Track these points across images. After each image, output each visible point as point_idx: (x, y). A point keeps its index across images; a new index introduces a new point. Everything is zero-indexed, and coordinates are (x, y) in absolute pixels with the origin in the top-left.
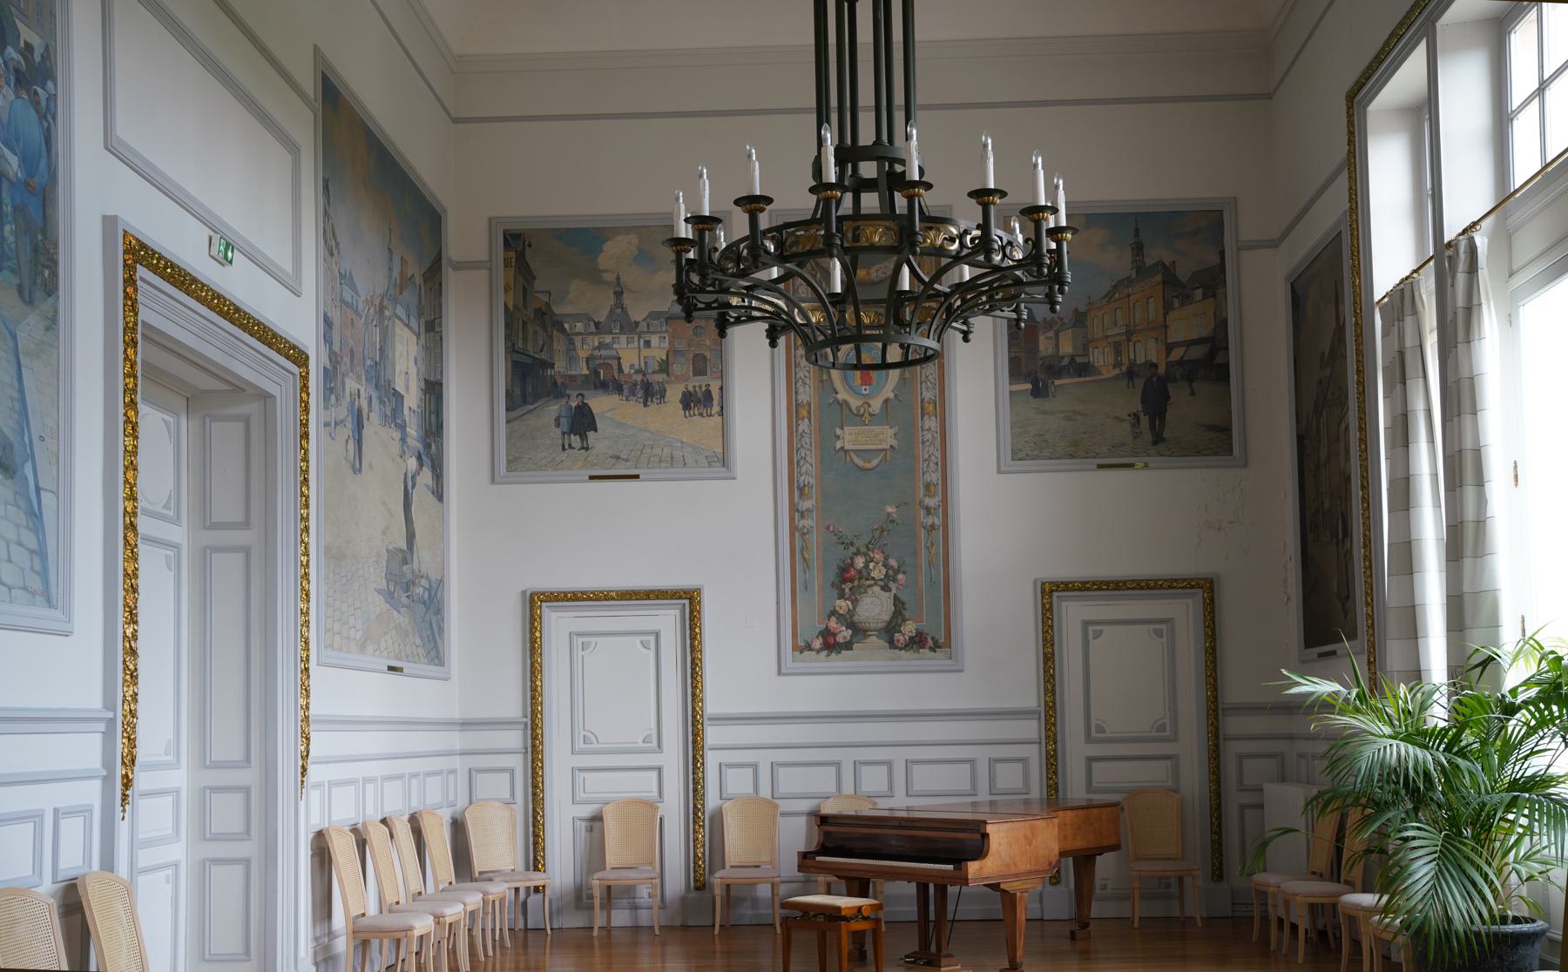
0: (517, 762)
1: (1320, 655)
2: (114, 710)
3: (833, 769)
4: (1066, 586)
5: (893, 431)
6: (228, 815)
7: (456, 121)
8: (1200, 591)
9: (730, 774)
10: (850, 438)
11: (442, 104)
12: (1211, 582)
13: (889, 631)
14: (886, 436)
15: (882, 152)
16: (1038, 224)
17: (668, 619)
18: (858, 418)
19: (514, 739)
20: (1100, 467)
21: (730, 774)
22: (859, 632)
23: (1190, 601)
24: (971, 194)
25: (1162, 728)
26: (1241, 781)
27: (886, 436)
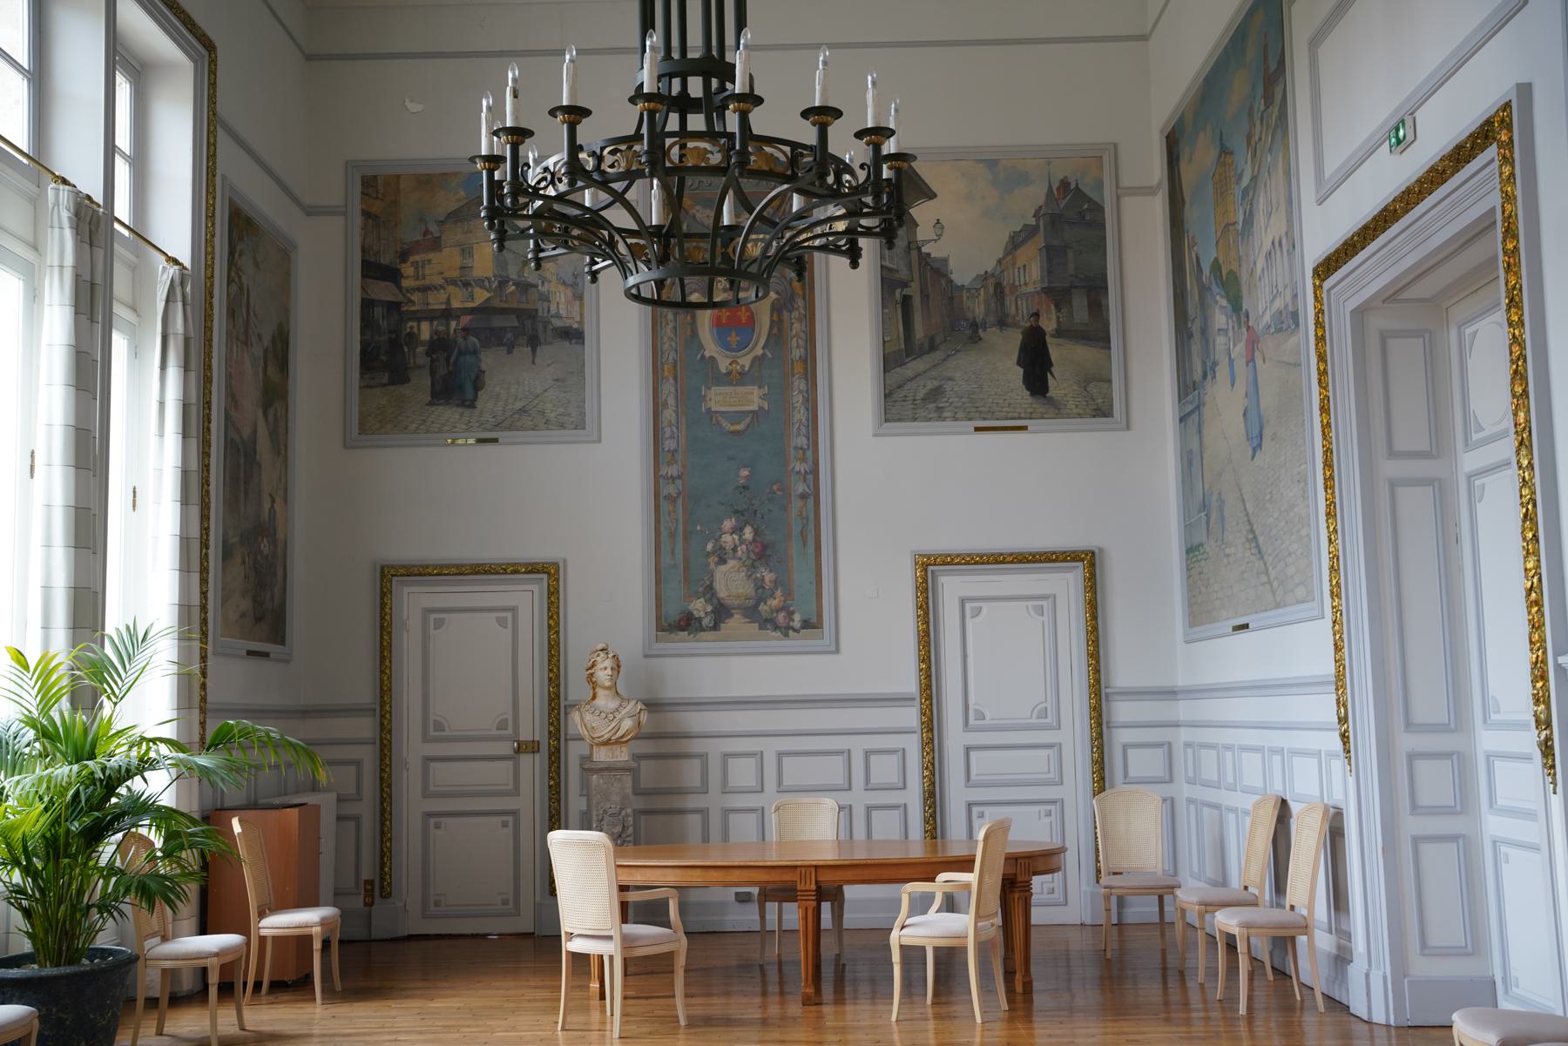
0: (912, 744)
1: (250, 653)
2: (1558, 666)
3: (873, 758)
4: (950, 561)
5: (762, 392)
6: (1435, 783)
7: (309, 58)
8: (545, 576)
9: (894, 760)
10: (719, 399)
11: (289, 33)
12: (556, 565)
13: (751, 613)
14: (752, 398)
15: (716, 67)
16: (877, 148)
17: (952, 587)
18: (730, 379)
19: (910, 716)
20: (977, 429)
21: (894, 760)
22: (721, 613)
23: (535, 588)
24: (806, 114)
25: (1044, 713)
26: (780, 782)
27: (752, 398)
